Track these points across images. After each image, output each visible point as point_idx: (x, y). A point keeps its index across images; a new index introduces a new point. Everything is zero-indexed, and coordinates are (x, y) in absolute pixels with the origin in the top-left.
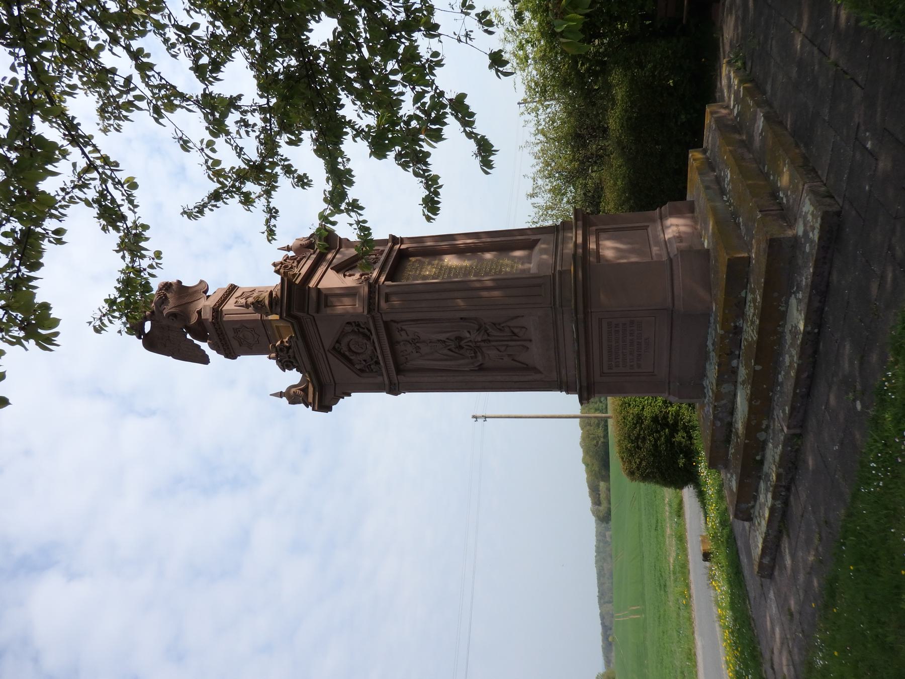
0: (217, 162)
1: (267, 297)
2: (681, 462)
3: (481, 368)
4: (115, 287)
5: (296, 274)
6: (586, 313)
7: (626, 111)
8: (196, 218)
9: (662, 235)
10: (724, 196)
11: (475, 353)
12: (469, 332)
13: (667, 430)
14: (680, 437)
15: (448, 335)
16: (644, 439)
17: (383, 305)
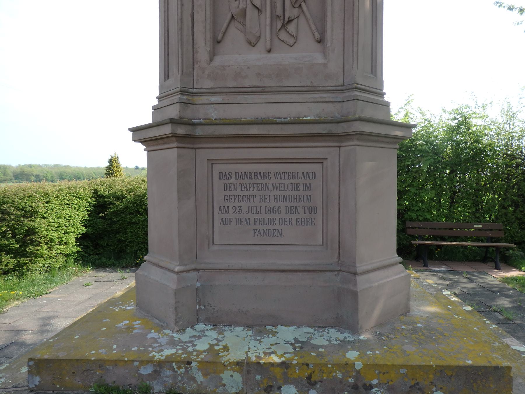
13: (17, 246)
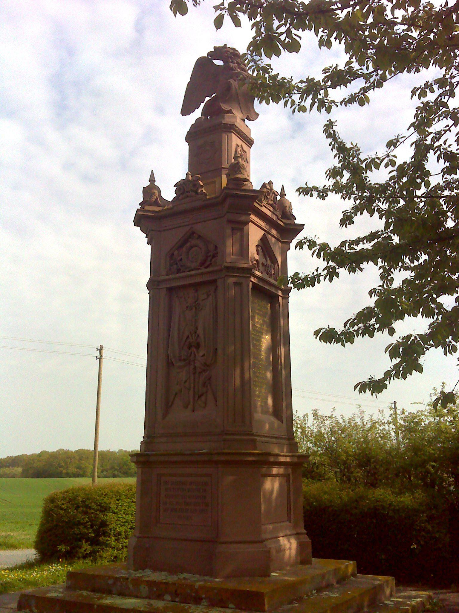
0: (377, 167)
1: (244, 177)
2: (63, 548)
3: (170, 364)
4: (278, 74)
5: (262, 203)
6: (216, 463)
7: (390, 505)
8: (325, 131)
9: (282, 535)
10: (316, 591)
11: (184, 360)
12: (204, 355)
14: (86, 547)
15: (202, 336)
16: (85, 513)
17: (231, 280)
